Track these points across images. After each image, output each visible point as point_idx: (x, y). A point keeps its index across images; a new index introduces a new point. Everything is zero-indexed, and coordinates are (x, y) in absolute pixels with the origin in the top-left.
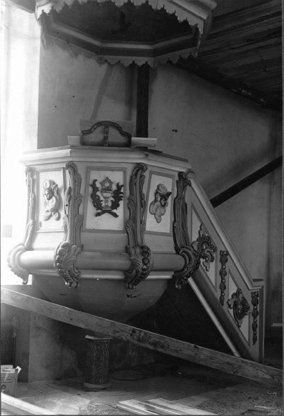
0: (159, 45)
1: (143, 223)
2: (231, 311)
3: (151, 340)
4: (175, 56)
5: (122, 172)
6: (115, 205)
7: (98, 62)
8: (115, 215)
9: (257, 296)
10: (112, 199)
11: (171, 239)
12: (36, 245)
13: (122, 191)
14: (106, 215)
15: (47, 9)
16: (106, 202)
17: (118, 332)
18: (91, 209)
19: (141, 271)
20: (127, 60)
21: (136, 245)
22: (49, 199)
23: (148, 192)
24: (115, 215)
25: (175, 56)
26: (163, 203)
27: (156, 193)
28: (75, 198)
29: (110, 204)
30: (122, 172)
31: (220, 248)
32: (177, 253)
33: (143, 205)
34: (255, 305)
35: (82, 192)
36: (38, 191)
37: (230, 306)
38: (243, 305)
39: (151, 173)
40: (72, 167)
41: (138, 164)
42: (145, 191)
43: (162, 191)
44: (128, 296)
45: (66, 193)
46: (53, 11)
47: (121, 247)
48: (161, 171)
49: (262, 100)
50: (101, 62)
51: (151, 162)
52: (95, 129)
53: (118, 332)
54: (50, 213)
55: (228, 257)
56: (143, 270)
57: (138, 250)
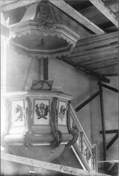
0: (53, 51)
1: (57, 121)
2: (85, 157)
3: (69, 170)
4: (60, 55)
5: (48, 101)
6: (46, 114)
7: (28, 56)
8: (46, 119)
9: (94, 150)
10: (44, 112)
11: (67, 127)
12: (10, 132)
13: (48, 108)
14: (42, 119)
15: (14, 36)
16: (42, 113)
17: (54, 168)
18: (36, 116)
19: (59, 141)
20: (40, 56)
21: (55, 131)
22: (17, 112)
23: (58, 109)
24: (46, 119)
25: (60, 55)
26: (64, 113)
27: (61, 109)
28: (29, 112)
29: (44, 114)
30: (48, 101)
31: (80, 131)
32: (70, 133)
33: (57, 114)
34: (93, 154)
35: (32, 109)
36: (11, 110)
37: (85, 155)
38: (89, 154)
39: (60, 101)
40: (28, 99)
41: (55, 97)
42: (57, 108)
43: (63, 108)
44: (51, 153)
45: (25, 109)
46: (17, 37)
47: (49, 131)
48: (63, 100)
49: (88, 72)
50: (29, 56)
51: (60, 97)
52: (38, 83)
53: (54, 168)
54: (17, 118)
55: (83, 134)
56: (60, 141)
57: (57, 133)
